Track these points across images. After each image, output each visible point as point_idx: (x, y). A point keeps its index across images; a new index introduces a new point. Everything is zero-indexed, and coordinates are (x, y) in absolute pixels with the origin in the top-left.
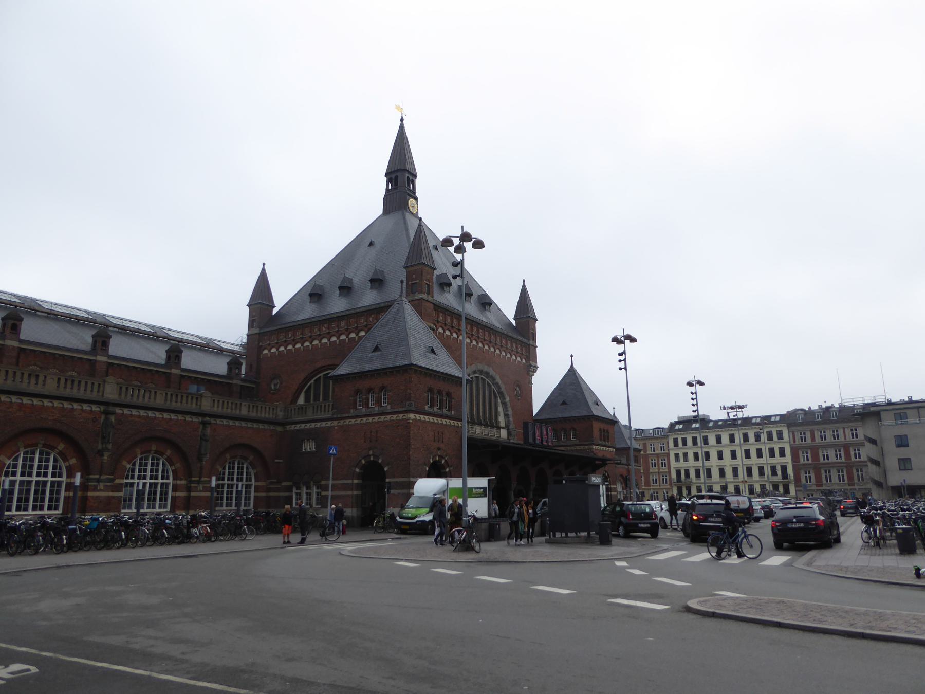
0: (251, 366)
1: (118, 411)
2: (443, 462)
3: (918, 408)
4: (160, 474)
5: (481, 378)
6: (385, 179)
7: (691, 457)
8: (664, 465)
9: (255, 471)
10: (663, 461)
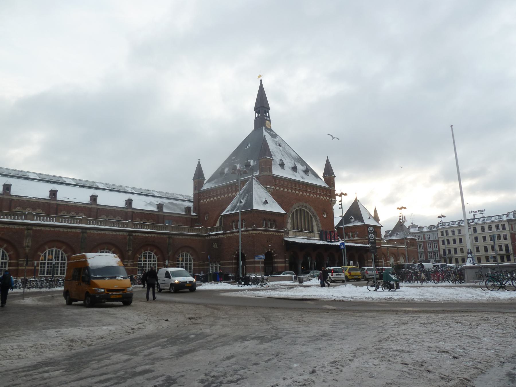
0: (196, 208)
1: (134, 234)
2: (273, 251)
4: (152, 259)
5: (303, 209)
6: (254, 111)
7: (451, 241)
8: (435, 247)
9: (193, 257)
10: (435, 245)
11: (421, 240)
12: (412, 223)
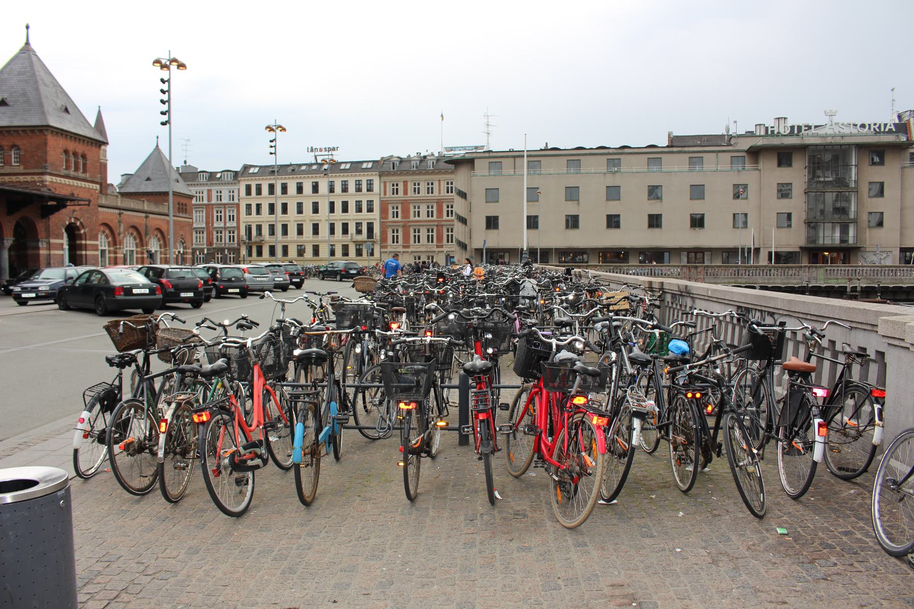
3: (514, 157)
7: (265, 209)
8: (231, 218)
11: (201, 202)
12: (185, 162)
